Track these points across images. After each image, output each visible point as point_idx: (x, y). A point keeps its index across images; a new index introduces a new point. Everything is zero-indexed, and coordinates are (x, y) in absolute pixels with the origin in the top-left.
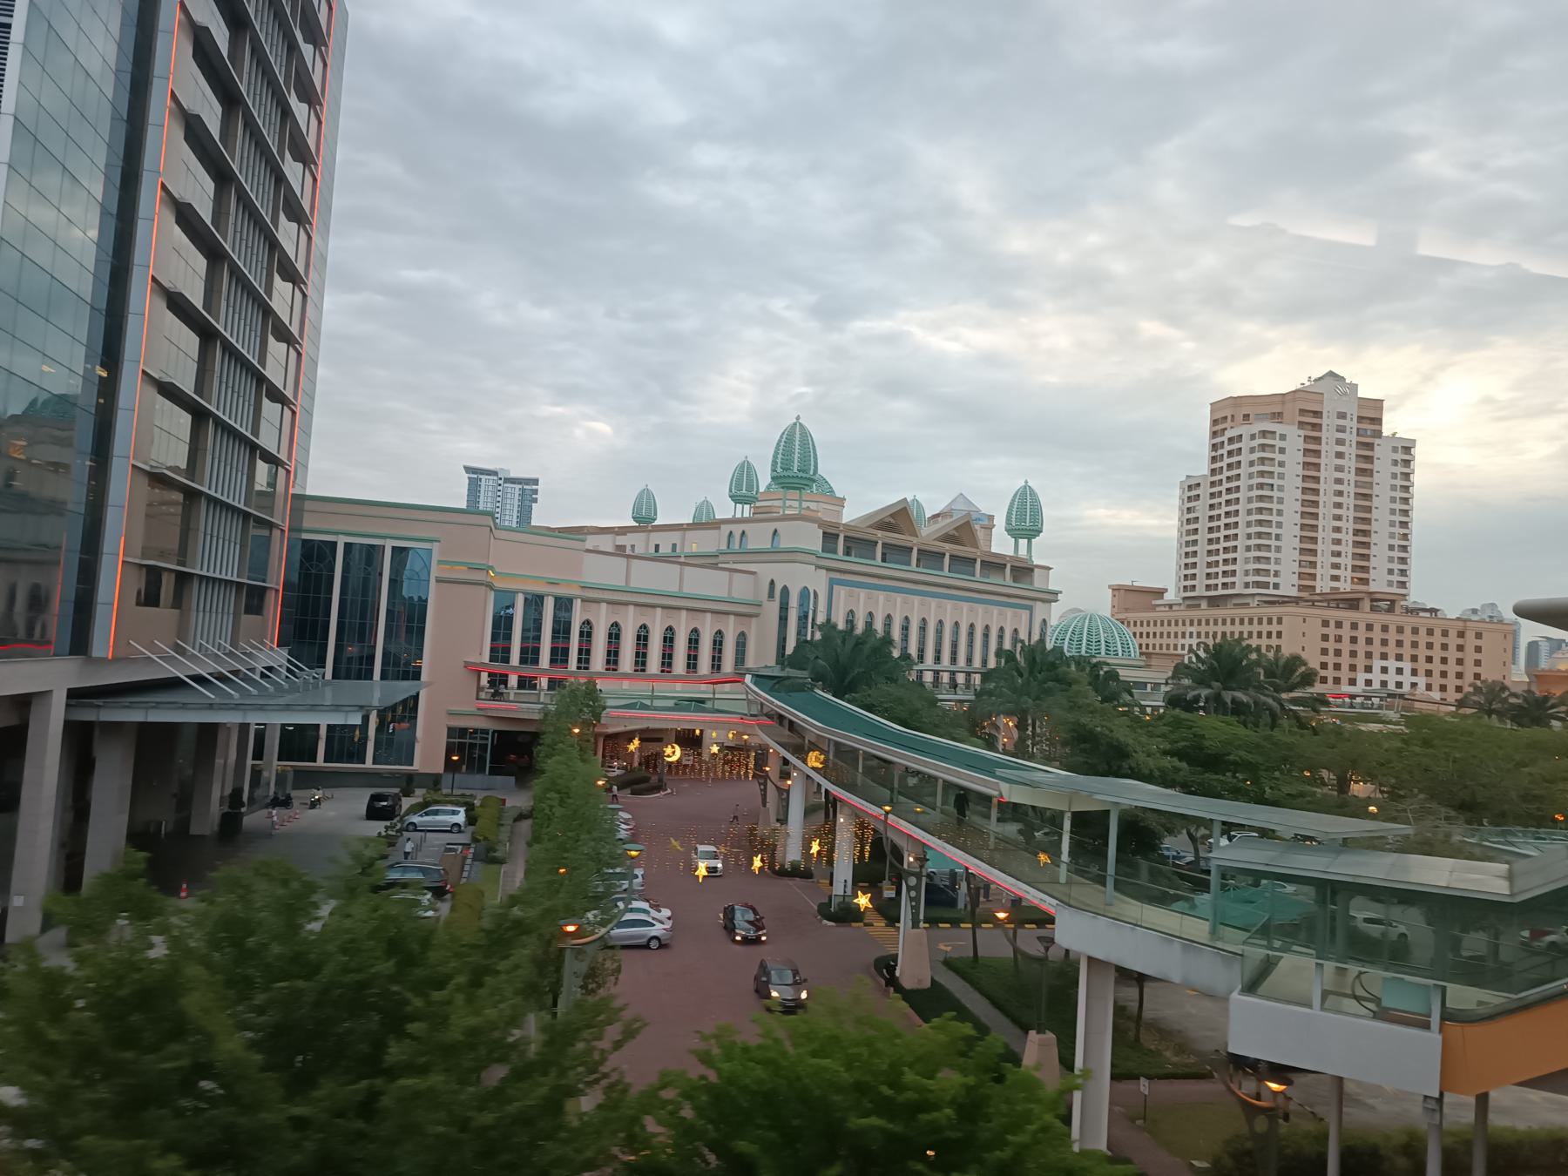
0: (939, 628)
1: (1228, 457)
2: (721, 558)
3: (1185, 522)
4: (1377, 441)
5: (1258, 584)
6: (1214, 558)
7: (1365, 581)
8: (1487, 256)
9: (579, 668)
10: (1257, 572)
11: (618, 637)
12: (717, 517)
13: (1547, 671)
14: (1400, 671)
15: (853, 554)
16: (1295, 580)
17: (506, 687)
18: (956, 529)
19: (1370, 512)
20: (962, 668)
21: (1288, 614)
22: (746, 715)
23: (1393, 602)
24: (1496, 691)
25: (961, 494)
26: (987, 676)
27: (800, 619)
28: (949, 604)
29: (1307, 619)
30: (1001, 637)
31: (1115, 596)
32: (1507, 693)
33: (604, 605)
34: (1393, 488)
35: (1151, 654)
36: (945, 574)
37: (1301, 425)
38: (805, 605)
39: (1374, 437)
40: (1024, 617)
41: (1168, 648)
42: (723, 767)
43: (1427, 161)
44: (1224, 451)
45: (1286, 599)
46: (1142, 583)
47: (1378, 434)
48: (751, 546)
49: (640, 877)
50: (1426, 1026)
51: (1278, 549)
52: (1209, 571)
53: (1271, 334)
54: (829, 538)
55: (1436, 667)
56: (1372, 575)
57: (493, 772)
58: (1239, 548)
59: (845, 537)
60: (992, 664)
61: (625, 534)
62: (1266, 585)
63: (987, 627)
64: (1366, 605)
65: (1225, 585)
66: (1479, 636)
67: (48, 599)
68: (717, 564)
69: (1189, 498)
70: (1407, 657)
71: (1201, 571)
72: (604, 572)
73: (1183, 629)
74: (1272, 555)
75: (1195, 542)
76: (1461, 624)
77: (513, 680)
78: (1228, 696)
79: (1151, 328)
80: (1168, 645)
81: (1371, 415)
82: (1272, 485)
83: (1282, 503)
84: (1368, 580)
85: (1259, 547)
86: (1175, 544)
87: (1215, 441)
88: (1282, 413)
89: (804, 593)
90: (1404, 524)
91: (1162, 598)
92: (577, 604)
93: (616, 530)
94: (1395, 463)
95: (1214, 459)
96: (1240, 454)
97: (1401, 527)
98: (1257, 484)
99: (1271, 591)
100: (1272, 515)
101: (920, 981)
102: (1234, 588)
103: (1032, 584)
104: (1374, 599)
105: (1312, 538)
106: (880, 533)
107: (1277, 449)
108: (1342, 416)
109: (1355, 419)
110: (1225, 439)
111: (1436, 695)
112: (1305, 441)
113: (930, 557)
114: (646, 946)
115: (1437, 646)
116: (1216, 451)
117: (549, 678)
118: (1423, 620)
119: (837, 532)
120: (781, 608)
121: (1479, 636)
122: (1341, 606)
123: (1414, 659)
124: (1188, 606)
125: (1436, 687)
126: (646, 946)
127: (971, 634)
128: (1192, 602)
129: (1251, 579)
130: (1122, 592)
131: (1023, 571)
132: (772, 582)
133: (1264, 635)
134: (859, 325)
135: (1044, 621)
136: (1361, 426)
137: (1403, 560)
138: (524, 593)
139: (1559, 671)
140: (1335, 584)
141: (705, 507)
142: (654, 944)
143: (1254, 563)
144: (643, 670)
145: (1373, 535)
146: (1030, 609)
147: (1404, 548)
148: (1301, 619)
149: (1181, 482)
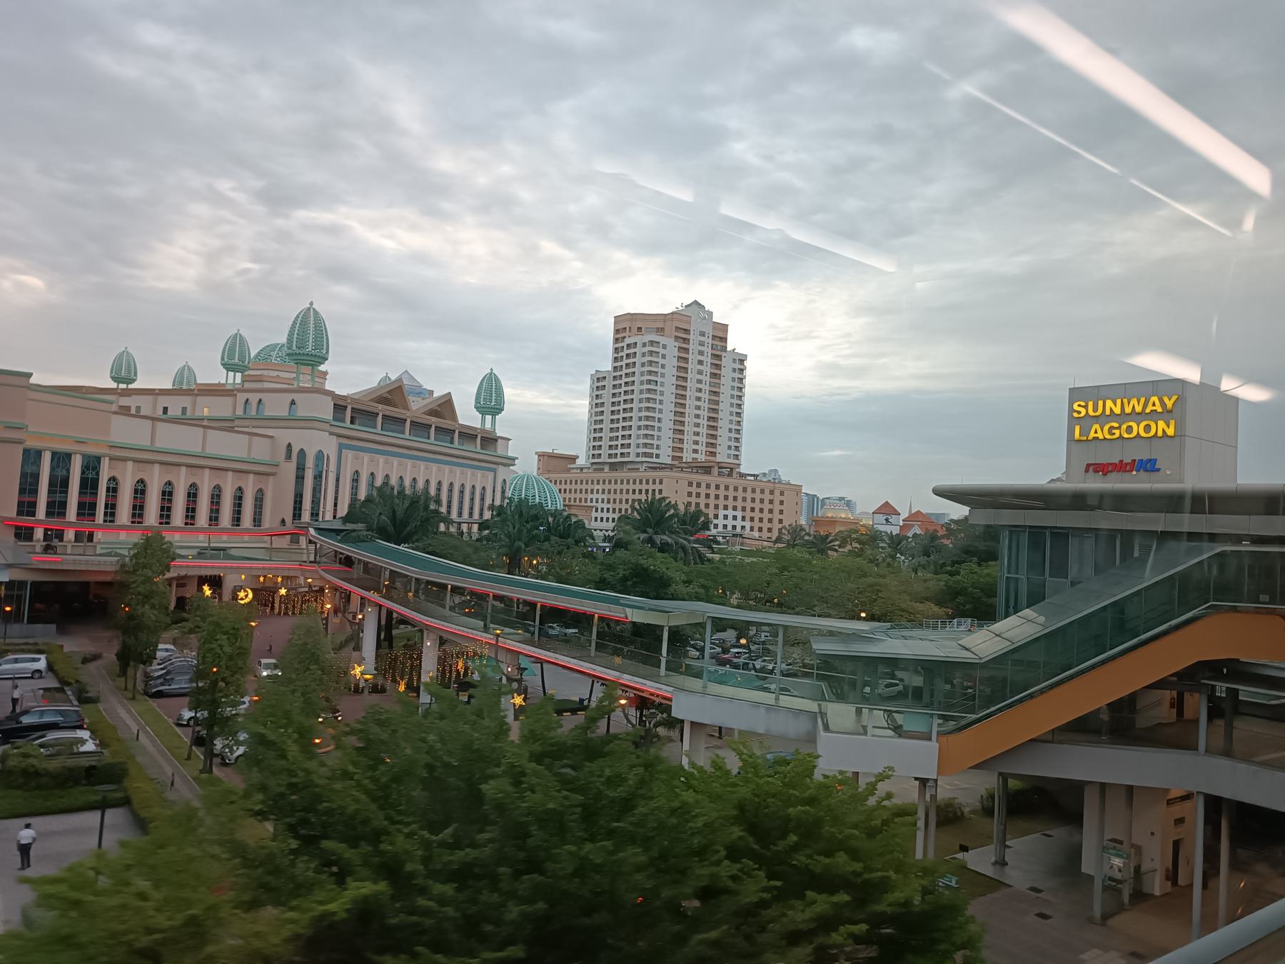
1: (626, 359)
2: (237, 423)
3: (594, 405)
4: (724, 354)
5: (645, 455)
6: (615, 434)
7: (713, 454)
8: (770, 223)
9: (105, 521)
10: (645, 445)
11: (143, 492)
12: (198, 382)
13: (843, 519)
14: (735, 518)
15: (357, 423)
17: (61, 540)
19: (718, 404)
20: (465, 519)
22: (305, 562)
23: (732, 469)
24: (796, 531)
25: (406, 371)
26: (483, 525)
27: (315, 478)
28: (434, 467)
31: (540, 460)
32: (804, 533)
33: (130, 464)
34: (733, 388)
35: (571, 505)
36: (432, 442)
38: (320, 465)
40: (490, 477)
41: (580, 501)
42: (302, 606)
43: (740, 149)
44: (624, 354)
45: (664, 466)
48: (268, 413)
49: (247, 702)
51: (659, 430)
52: (611, 443)
53: (636, 263)
56: (719, 449)
57: (32, 620)
58: (633, 427)
59: (352, 408)
60: (487, 515)
61: (130, 395)
62: (650, 455)
63: (451, 484)
64: (715, 471)
66: (782, 493)
67: (384, 493)
68: (233, 428)
69: (597, 387)
70: (739, 508)
71: (605, 443)
73: (592, 487)
75: (601, 421)
76: (772, 485)
77: (70, 535)
78: (658, 539)
79: (549, 247)
80: (580, 499)
81: (720, 334)
82: (657, 382)
85: (647, 427)
87: (617, 346)
89: (320, 456)
90: (739, 414)
91: (575, 463)
92: (105, 463)
94: (734, 370)
95: (616, 359)
96: (635, 357)
98: (647, 380)
99: (654, 460)
102: (600, 458)
103: (496, 451)
106: (380, 407)
108: (703, 334)
109: (711, 337)
110: (624, 344)
111: (756, 534)
112: (678, 350)
117: (76, 531)
119: (345, 404)
120: (297, 468)
121: (782, 493)
123: (744, 509)
127: (462, 492)
128: (598, 467)
130: (546, 457)
131: (490, 440)
134: (303, 215)
136: (715, 342)
137: (737, 440)
138: (81, 454)
139: (827, 517)
140: (695, 456)
141: (185, 372)
143: (643, 439)
144: (168, 523)
145: (720, 421)
146: (495, 471)
147: (738, 431)
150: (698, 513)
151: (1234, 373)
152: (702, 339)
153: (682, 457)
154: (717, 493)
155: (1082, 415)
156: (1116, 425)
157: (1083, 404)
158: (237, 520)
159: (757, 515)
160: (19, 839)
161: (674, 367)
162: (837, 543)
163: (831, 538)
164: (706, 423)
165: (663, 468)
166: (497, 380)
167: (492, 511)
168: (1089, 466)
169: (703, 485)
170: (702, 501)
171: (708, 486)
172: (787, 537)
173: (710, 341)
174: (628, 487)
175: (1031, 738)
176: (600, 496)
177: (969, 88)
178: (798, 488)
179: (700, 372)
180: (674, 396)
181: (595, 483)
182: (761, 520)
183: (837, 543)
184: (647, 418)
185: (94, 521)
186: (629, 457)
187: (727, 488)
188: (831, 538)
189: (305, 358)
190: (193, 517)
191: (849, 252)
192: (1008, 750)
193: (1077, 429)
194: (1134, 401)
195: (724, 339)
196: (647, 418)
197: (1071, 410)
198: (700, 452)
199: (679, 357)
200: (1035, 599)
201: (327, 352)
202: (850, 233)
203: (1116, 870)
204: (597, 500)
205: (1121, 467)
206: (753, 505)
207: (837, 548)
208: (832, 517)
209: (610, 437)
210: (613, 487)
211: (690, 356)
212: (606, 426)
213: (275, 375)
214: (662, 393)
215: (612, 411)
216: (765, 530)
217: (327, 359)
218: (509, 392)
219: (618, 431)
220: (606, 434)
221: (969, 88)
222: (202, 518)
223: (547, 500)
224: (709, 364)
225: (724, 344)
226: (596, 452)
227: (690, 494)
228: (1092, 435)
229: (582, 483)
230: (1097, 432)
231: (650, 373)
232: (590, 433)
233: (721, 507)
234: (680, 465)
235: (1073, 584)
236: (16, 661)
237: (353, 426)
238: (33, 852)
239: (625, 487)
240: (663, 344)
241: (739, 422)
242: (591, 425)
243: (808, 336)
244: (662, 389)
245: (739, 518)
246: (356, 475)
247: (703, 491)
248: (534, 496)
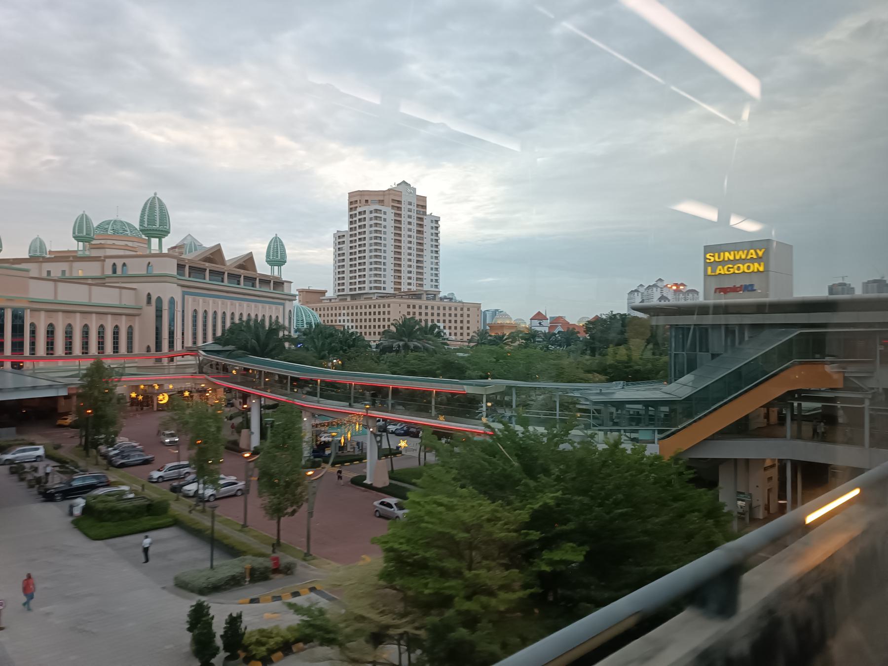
0: (205, 315)
2: (107, 280)
4: (425, 217)
5: (376, 288)
7: (421, 285)
10: (376, 281)
16: (392, 285)
18: (244, 262)
21: (394, 303)
23: (435, 295)
25: (189, 235)
29: (401, 305)
30: (232, 319)
32: (488, 335)
39: (423, 215)
43: (415, 69)
44: (357, 219)
46: (314, 288)
47: (425, 213)
48: (130, 273)
50: (654, 443)
51: (385, 270)
54: (180, 267)
56: (425, 282)
62: (379, 288)
63: (215, 312)
64: (424, 296)
66: (468, 310)
68: (104, 283)
71: (347, 281)
72: (41, 291)
74: (382, 273)
76: (461, 304)
79: (281, 140)
81: (422, 204)
82: (381, 237)
83: (386, 247)
84: (423, 284)
85: (376, 269)
86: (332, 268)
88: (384, 200)
91: (324, 296)
93: (11, 261)
94: (432, 228)
95: (351, 223)
97: (435, 259)
100: (381, 252)
101: (385, 483)
103: (283, 291)
105: (399, 264)
108: (410, 204)
109: (416, 205)
110: (357, 212)
111: (459, 337)
113: (234, 277)
114: (235, 495)
116: (352, 219)
118: (446, 303)
121: (468, 310)
122: (413, 298)
124: (340, 300)
126: (235, 495)
127: (215, 318)
128: (342, 298)
129: (373, 285)
131: (279, 284)
132: (149, 295)
133: (377, 313)
134: (90, 118)
136: (418, 209)
137: (436, 275)
139: (498, 324)
140: (409, 287)
142: (239, 493)
145: (424, 263)
146: (283, 304)
148: (399, 305)
149: (334, 234)
150: (434, 326)
151: (739, 214)
152: (410, 207)
154: (414, 311)
155: (712, 260)
156: (731, 266)
157: (712, 254)
158: (116, 348)
159: (453, 325)
160: (143, 545)
161: (392, 227)
162: (510, 340)
163: (505, 337)
164: (415, 264)
165: (389, 296)
166: (281, 242)
168: (716, 289)
169: (417, 307)
170: (435, 318)
171: (420, 307)
172: (477, 338)
173: (415, 208)
174: (361, 311)
175: (705, 438)
176: (346, 318)
177: (568, 26)
179: (410, 230)
180: (393, 247)
181: (342, 308)
182: (456, 328)
183: (510, 340)
184: (376, 263)
185: (23, 354)
186: (365, 290)
187: (433, 308)
188: (505, 337)
189: (152, 232)
190: (52, 349)
191: (492, 139)
192: (696, 445)
193: (709, 269)
194: (741, 253)
195: (424, 207)
196: (376, 263)
197: (706, 258)
198: (412, 284)
199: (395, 220)
200: (691, 367)
201: (170, 227)
202: (493, 128)
203: (739, 507)
204: (344, 321)
205: (734, 290)
206: (450, 318)
207: (510, 343)
208: (501, 324)
209: (350, 277)
210: (355, 311)
211: (403, 219)
212: (347, 269)
213: (111, 243)
214: (385, 245)
215: (351, 259)
216: (459, 334)
217: (169, 233)
218: (291, 252)
219: (356, 273)
220: (347, 275)
221: (568, 26)
222: (60, 349)
223: (303, 322)
224: (415, 224)
225: (424, 210)
226: (341, 288)
228: (718, 272)
229: (332, 309)
230: (721, 270)
231: (376, 231)
232: (336, 275)
234: (400, 294)
235: (714, 356)
236: (24, 451)
237: (190, 279)
238: (150, 552)
239: (363, 311)
240: (384, 212)
241: (437, 263)
242: (336, 269)
243: (466, 200)
244: (385, 242)
246: (195, 313)
248: (303, 320)
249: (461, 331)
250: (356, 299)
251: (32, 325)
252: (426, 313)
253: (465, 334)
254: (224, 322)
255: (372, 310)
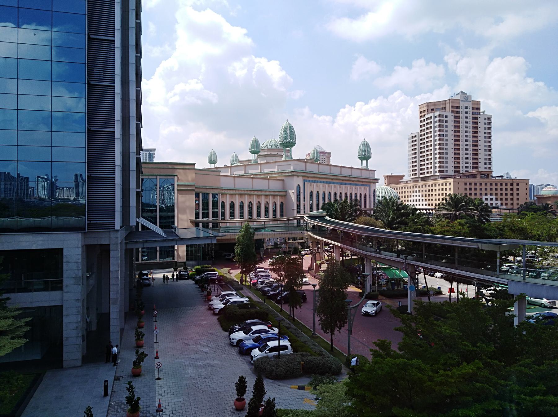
4: (479, 116)
7: (477, 168)
16: (453, 169)
19: (478, 142)
23: (488, 175)
37: (453, 112)
47: (479, 114)
55: (504, 197)
56: (480, 165)
65: (428, 172)
66: (518, 185)
70: (494, 194)
81: (476, 108)
82: (443, 135)
99: (445, 174)
104: (481, 174)
107: (445, 126)
109: (471, 109)
110: (425, 118)
111: (504, 207)
115: (499, 189)
121: (518, 185)
124: (414, 181)
125: (504, 204)
128: (415, 180)
130: (388, 178)
133: (430, 190)
135: (374, 190)
136: (474, 111)
146: (370, 186)
153: (460, 171)
167: (410, 208)
171: (476, 184)
174: (435, 188)
178: (527, 181)
195: (479, 109)
201: (296, 140)
227: (466, 189)
233: (484, 194)
245: (494, 199)
247: (473, 187)
249: (476, 187)
250: (425, 180)
251: (223, 203)
252: (490, 188)
253: (515, 204)
254: (324, 199)
255: (441, 187)
